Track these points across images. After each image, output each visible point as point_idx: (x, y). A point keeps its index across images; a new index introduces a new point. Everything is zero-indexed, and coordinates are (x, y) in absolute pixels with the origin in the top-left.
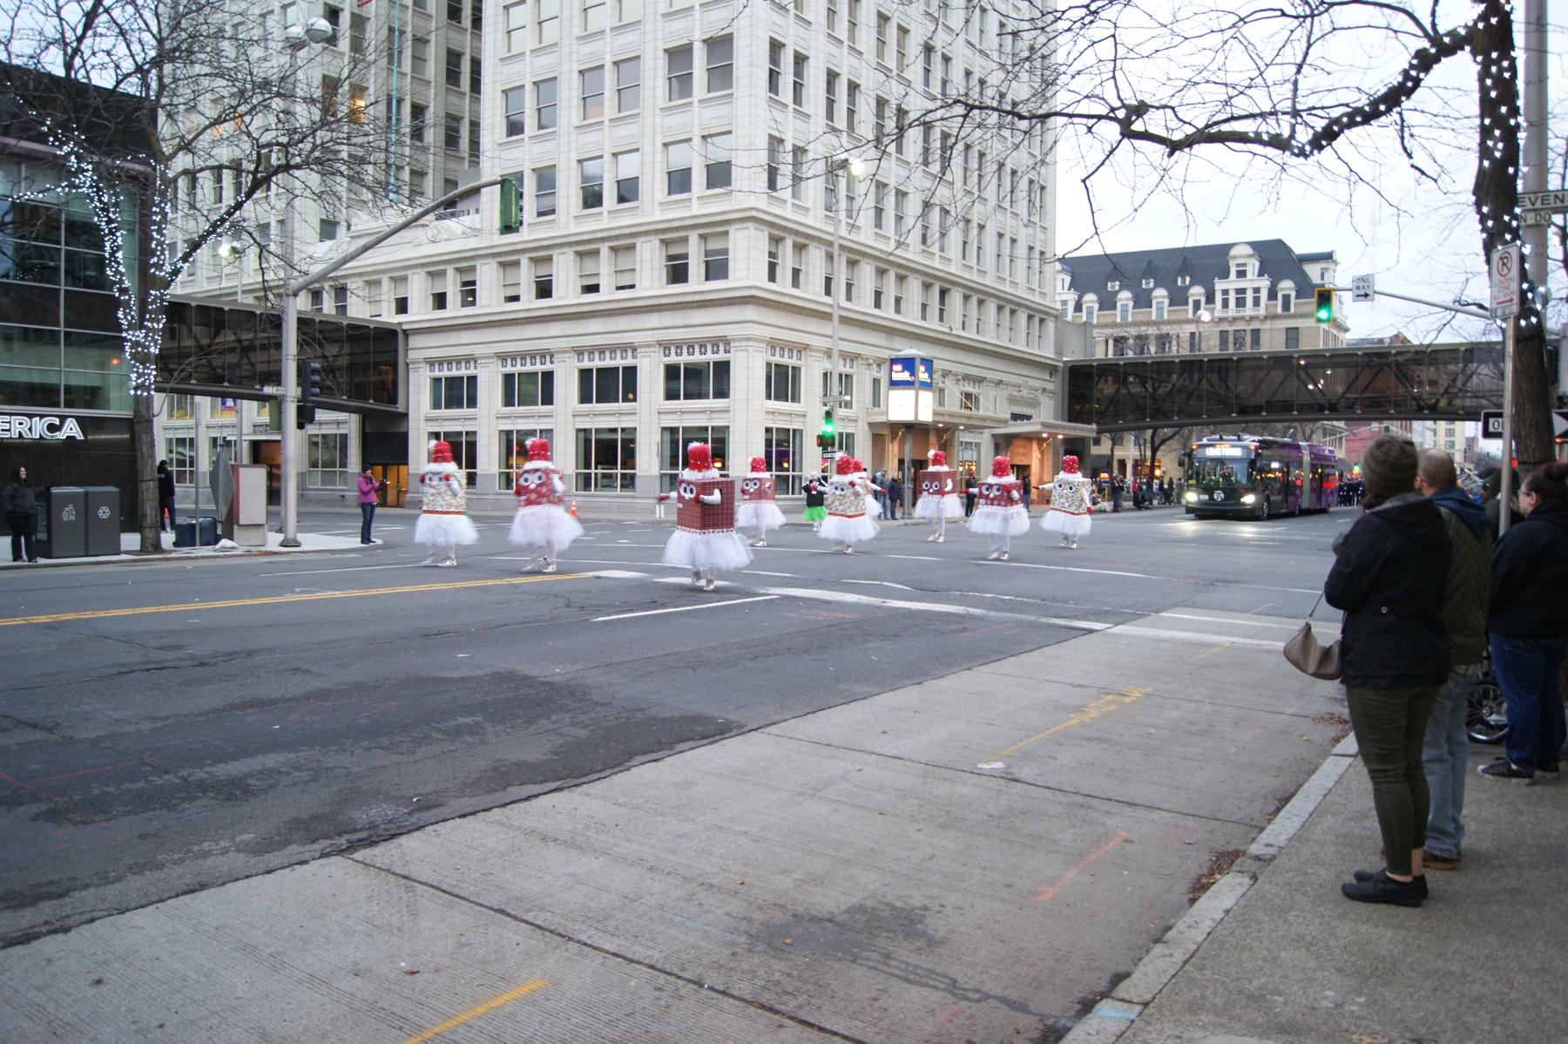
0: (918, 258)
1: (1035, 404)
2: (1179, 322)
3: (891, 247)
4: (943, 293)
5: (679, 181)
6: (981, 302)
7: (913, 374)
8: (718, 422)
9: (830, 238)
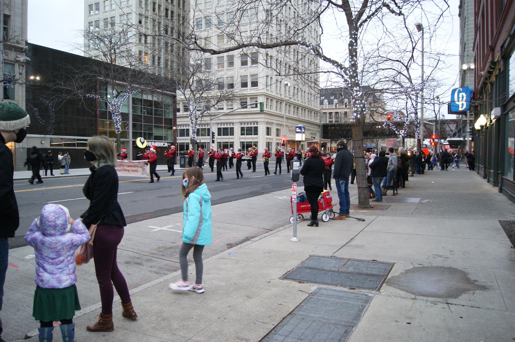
2: (341, 109)
3: (288, 99)
4: (297, 108)
5: (244, 85)
6: (271, 100)
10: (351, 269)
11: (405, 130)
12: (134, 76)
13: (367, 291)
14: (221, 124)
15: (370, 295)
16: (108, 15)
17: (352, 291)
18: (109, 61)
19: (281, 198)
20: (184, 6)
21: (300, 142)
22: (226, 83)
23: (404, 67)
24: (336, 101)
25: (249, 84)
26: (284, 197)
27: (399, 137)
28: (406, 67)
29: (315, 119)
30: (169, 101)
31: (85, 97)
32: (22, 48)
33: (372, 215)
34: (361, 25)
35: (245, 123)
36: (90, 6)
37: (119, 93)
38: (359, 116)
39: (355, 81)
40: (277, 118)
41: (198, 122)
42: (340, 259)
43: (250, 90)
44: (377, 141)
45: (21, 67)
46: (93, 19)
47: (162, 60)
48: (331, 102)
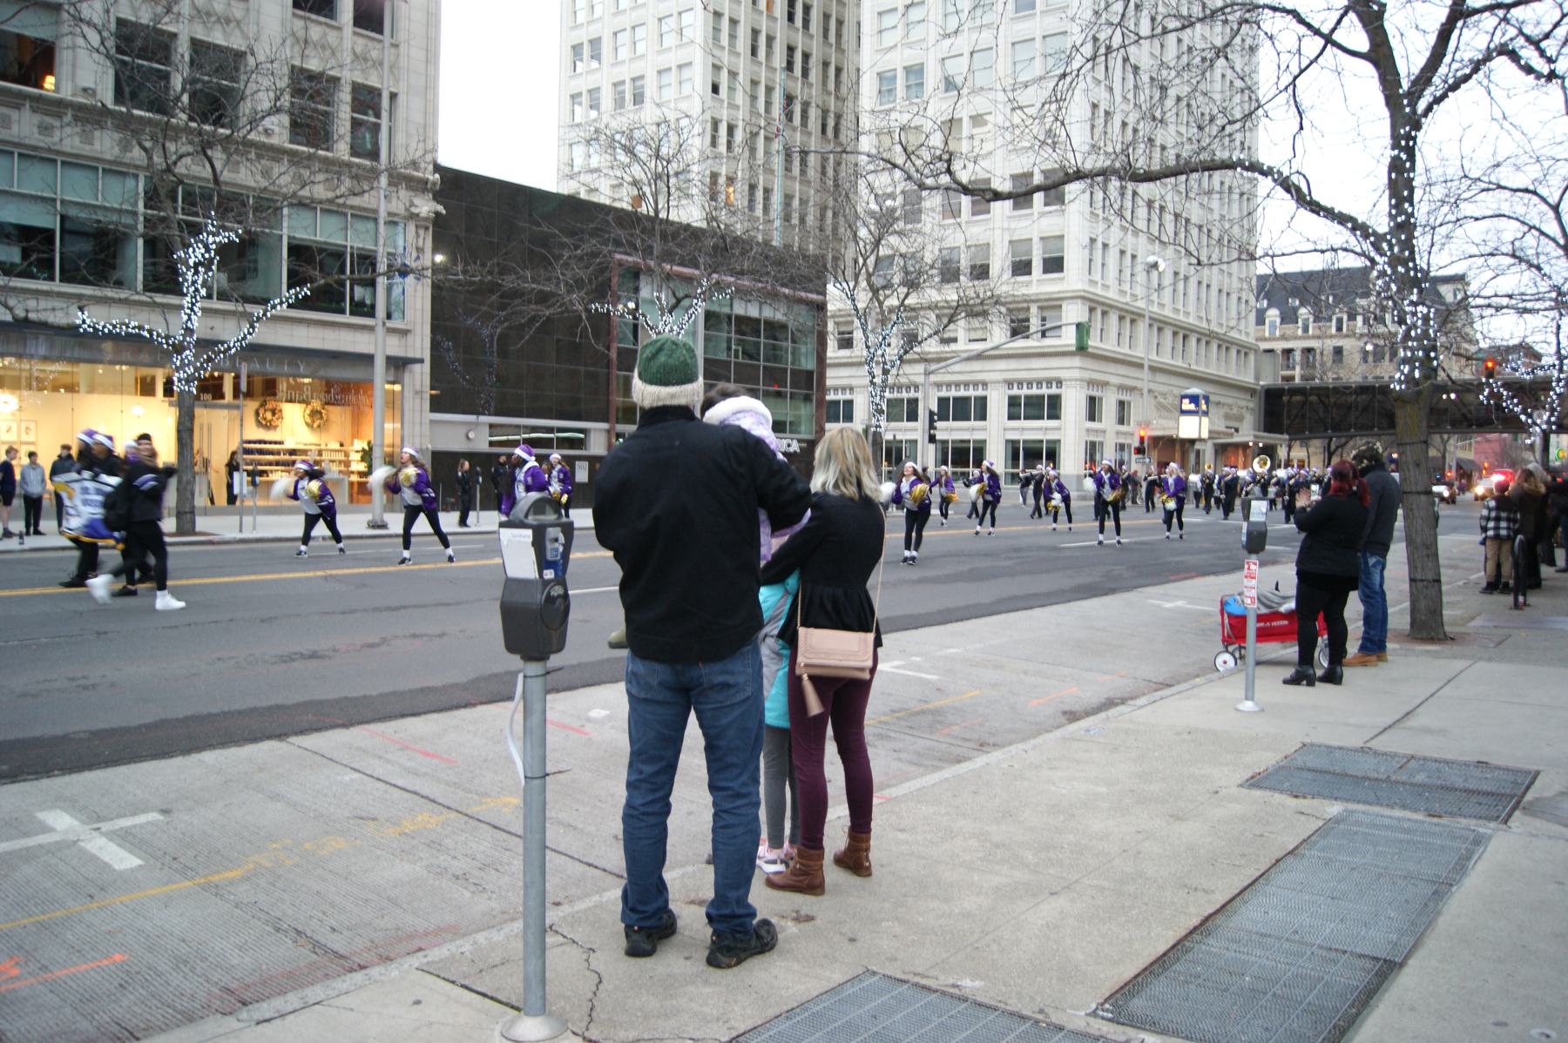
0: (1116, 297)
3: (1128, 299)
5: (1022, 268)
6: (1104, 313)
7: (1197, 405)
8: (1052, 436)
10: (1421, 778)
11: (1553, 410)
12: (714, 250)
13: (1474, 822)
14: (949, 385)
15: (1481, 830)
16: (626, 73)
17: (1435, 820)
18: (652, 213)
19: (1169, 605)
20: (839, 35)
21: (1192, 442)
22: (964, 264)
23: (1545, 208)
24: (1304, 312)
25: (1037, 265)
26: (1180, 603)
27: (1530, 435)
28: (1555, 208)
29: (1238, 373)
30: (802, 317)
31: (588, 311)
32: (426, 182)
33: (1454, 657)
34: (1429, 109)
35: (1020, 384)
36: (577, 49)
37: (679, 301)
38: (1417, 374)
39: (1408, 270)
40: (1122, 370)
41: (891, 380)
42: (1385, 754)
43: (1038, 284)
44: (1445, 443)
45: (421, 232)
46: (582, 85)
47: (777, 199)
48: (1289, 317)
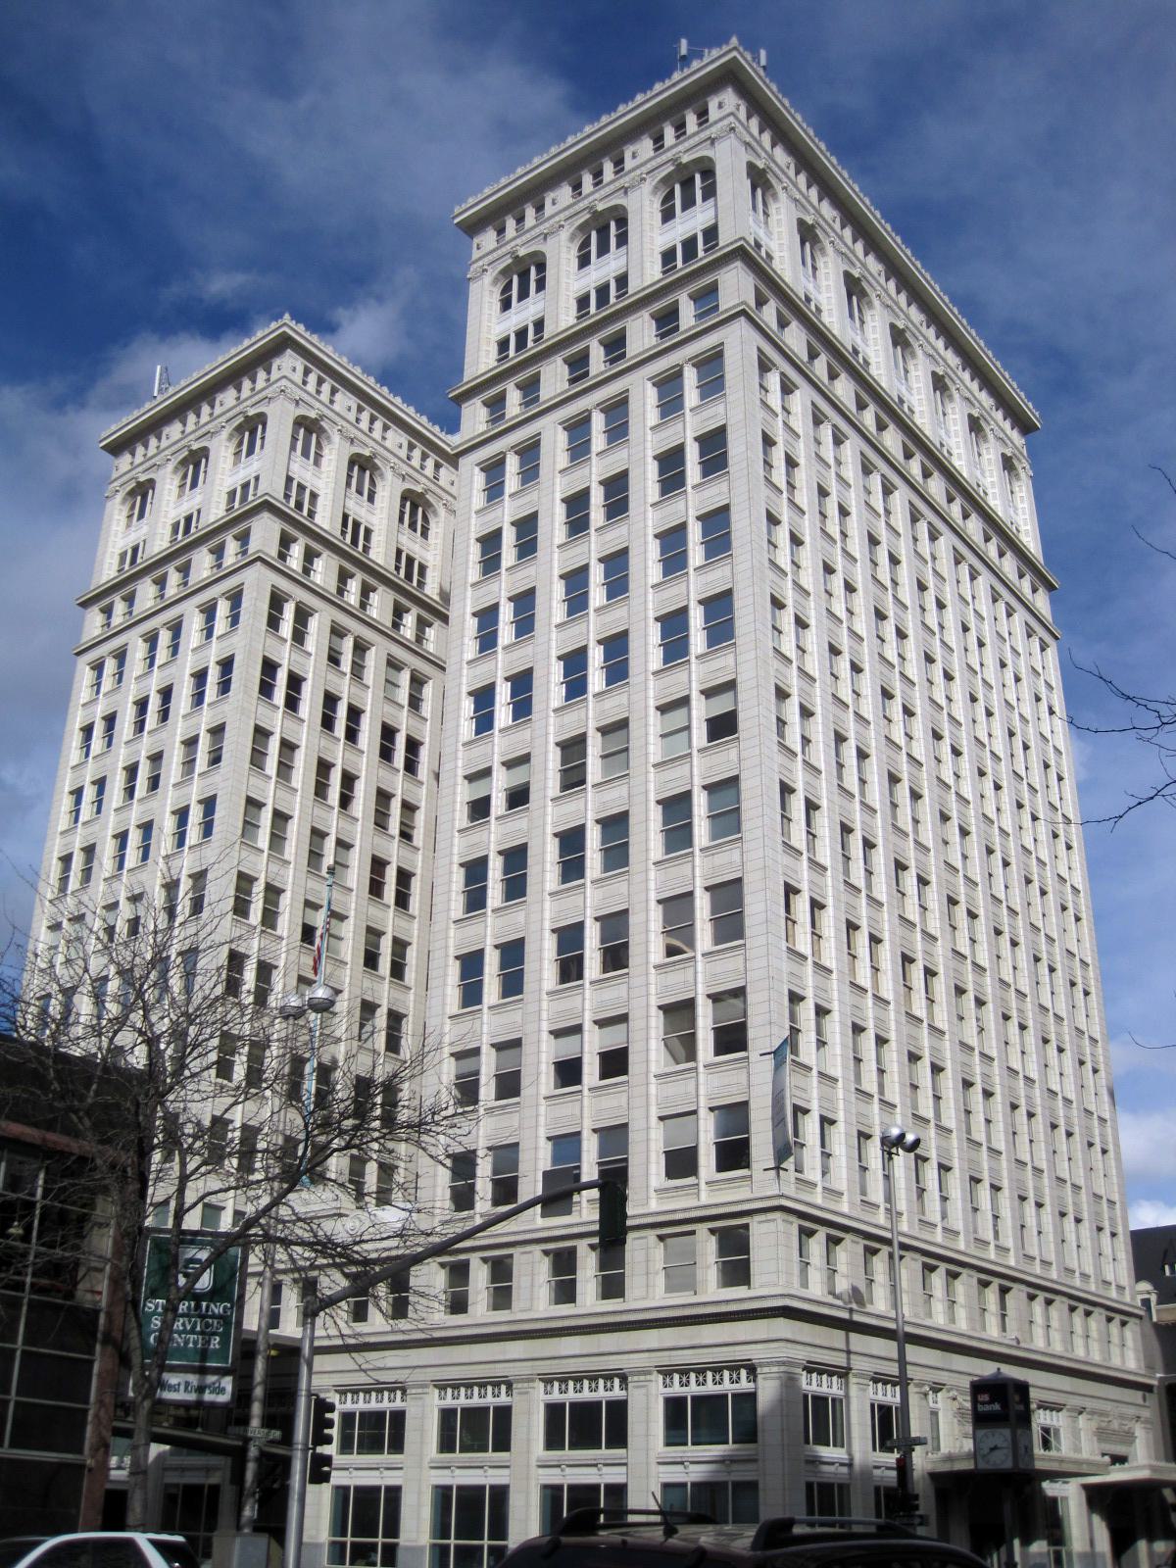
1: (1129, 1438)
9: (888, 1235)
